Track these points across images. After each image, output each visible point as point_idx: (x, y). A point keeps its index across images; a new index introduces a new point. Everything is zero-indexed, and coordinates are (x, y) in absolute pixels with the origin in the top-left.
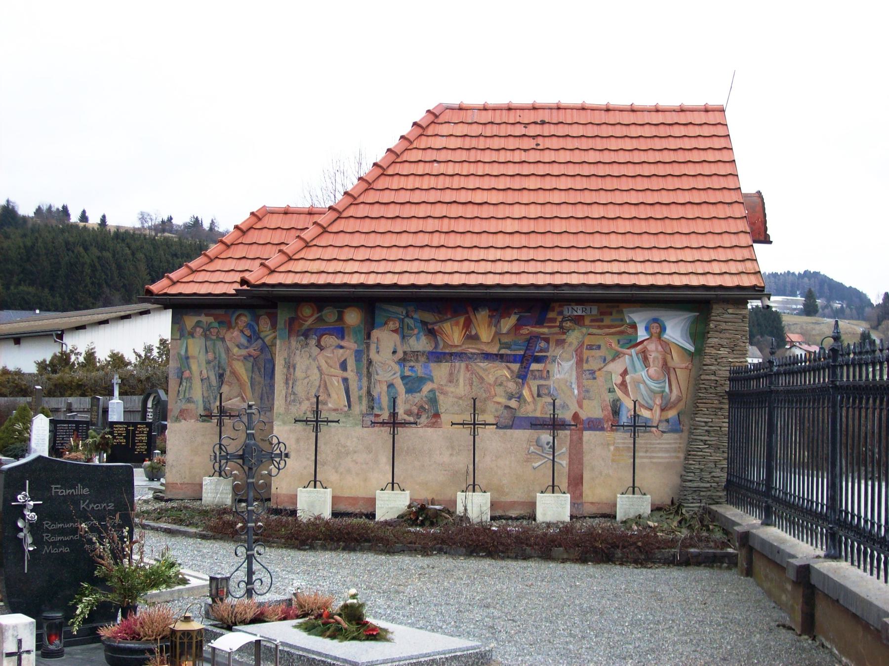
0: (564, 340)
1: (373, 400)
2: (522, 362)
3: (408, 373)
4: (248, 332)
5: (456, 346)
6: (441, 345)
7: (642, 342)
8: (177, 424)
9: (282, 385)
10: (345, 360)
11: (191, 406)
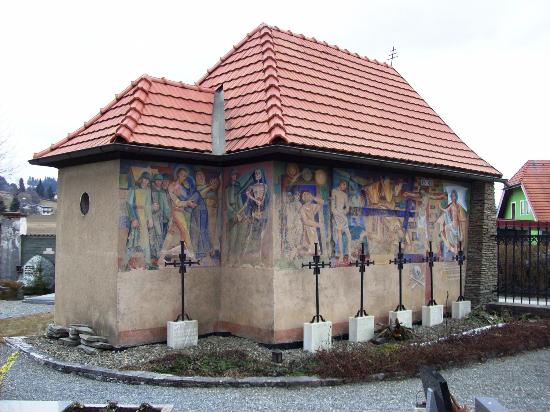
0: (421, 202)
1: (334, 245)
2: (405, 217)
3: (352, 224)
4: (187, 185)
5: (376, 204)
6: (368, 203)
7: (450, 205)
8: (127, 273)
9: (279, 234)
10: (318, 213)
11: (139, 254)
